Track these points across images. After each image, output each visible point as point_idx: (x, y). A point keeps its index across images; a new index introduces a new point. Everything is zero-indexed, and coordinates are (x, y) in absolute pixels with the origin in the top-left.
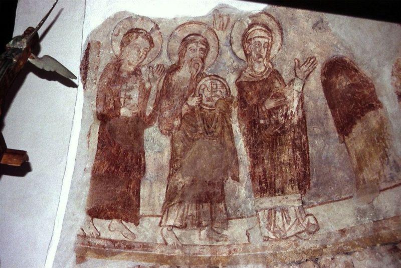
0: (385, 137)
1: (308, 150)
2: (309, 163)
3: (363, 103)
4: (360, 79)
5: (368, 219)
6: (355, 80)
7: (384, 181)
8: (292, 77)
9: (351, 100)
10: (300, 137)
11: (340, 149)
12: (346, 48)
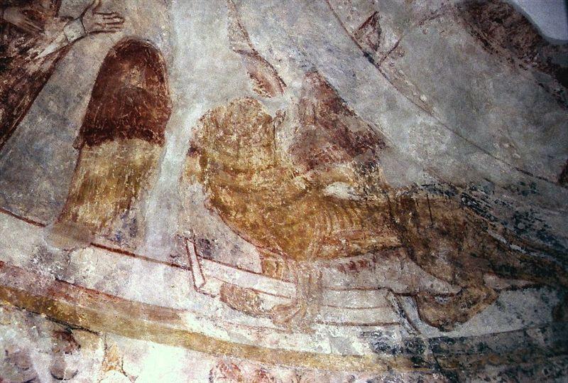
0: (141, 183)
1: (20, 120)
2: (8, 137)
3: (141, 123)
4: (158, 93)
5: (49, 269)
6: (152, 89)
7: (105, 236)
8: (76, 14)
9: (128, 108)
10: (22, 95)
11: (68, 154)
12: (171, 44)
